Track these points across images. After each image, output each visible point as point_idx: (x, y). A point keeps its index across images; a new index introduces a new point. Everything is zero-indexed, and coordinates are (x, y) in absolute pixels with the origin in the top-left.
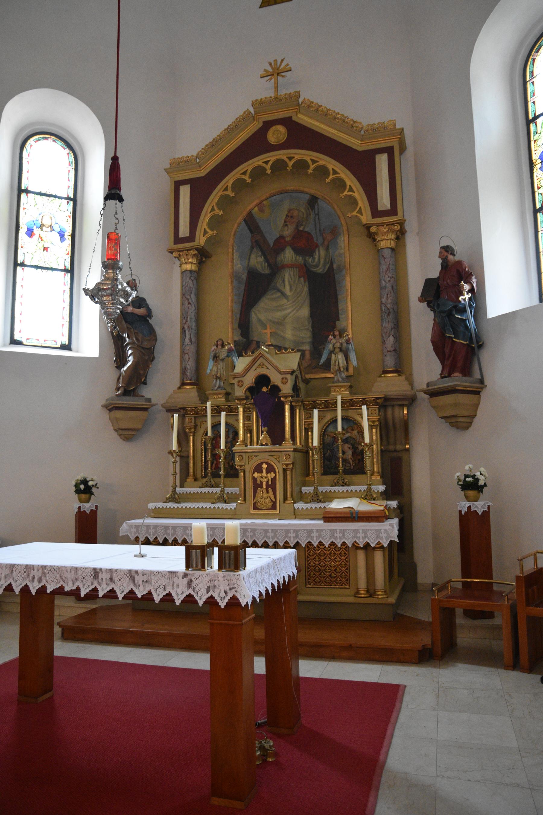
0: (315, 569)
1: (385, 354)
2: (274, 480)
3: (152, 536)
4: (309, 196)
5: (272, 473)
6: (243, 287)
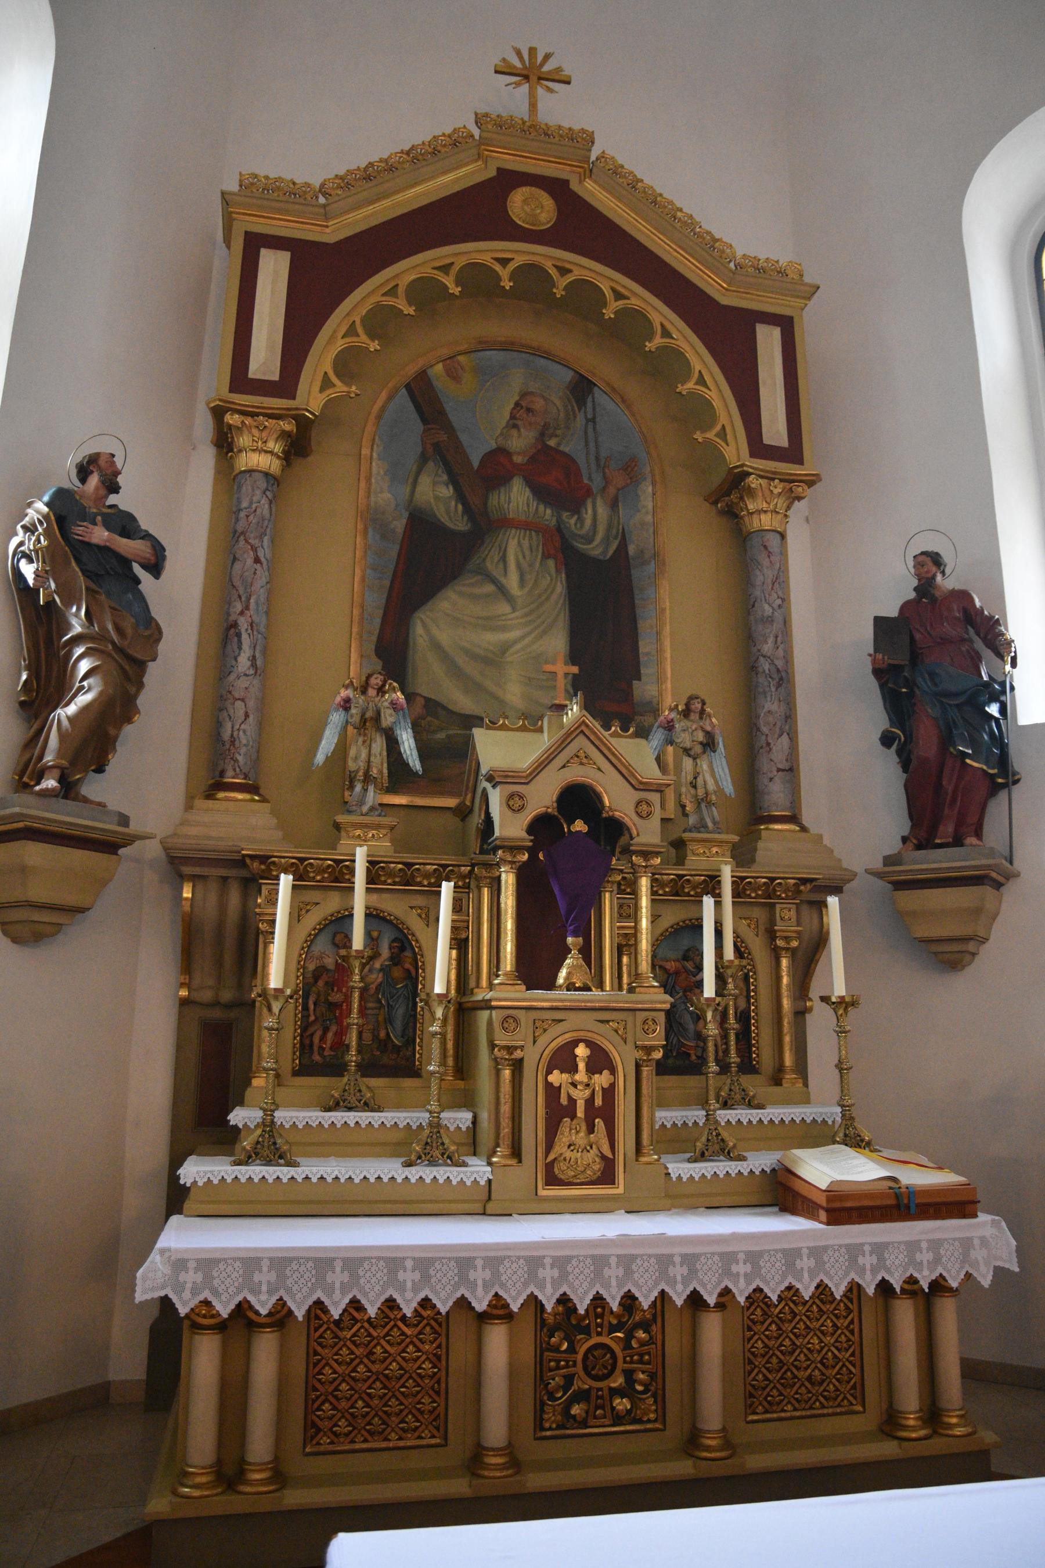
0: (768, 1362)
1: (770, 775)
2: (609, 1093)
3: (263, 1297)
4: (571, 374)
5: (606, 1072)
6: (394, 551)
